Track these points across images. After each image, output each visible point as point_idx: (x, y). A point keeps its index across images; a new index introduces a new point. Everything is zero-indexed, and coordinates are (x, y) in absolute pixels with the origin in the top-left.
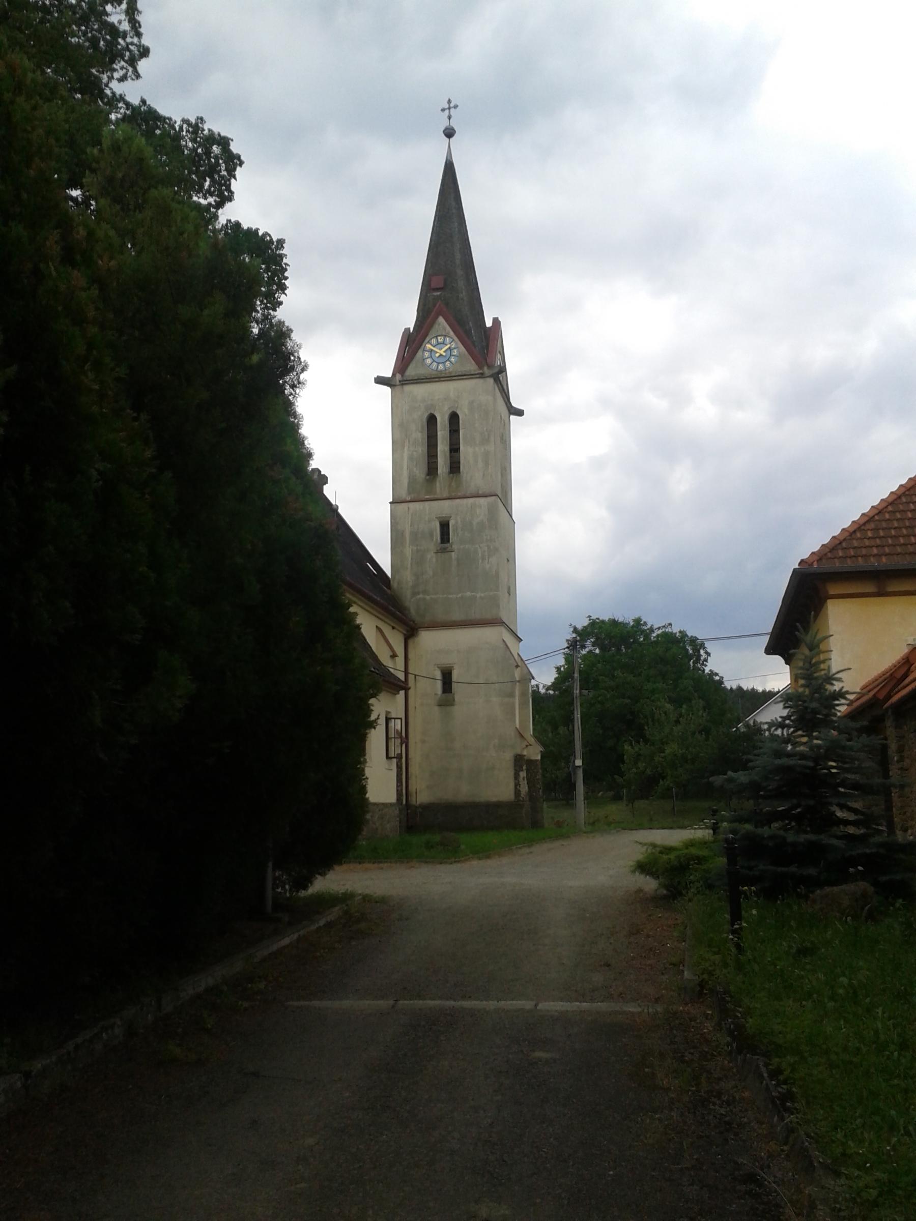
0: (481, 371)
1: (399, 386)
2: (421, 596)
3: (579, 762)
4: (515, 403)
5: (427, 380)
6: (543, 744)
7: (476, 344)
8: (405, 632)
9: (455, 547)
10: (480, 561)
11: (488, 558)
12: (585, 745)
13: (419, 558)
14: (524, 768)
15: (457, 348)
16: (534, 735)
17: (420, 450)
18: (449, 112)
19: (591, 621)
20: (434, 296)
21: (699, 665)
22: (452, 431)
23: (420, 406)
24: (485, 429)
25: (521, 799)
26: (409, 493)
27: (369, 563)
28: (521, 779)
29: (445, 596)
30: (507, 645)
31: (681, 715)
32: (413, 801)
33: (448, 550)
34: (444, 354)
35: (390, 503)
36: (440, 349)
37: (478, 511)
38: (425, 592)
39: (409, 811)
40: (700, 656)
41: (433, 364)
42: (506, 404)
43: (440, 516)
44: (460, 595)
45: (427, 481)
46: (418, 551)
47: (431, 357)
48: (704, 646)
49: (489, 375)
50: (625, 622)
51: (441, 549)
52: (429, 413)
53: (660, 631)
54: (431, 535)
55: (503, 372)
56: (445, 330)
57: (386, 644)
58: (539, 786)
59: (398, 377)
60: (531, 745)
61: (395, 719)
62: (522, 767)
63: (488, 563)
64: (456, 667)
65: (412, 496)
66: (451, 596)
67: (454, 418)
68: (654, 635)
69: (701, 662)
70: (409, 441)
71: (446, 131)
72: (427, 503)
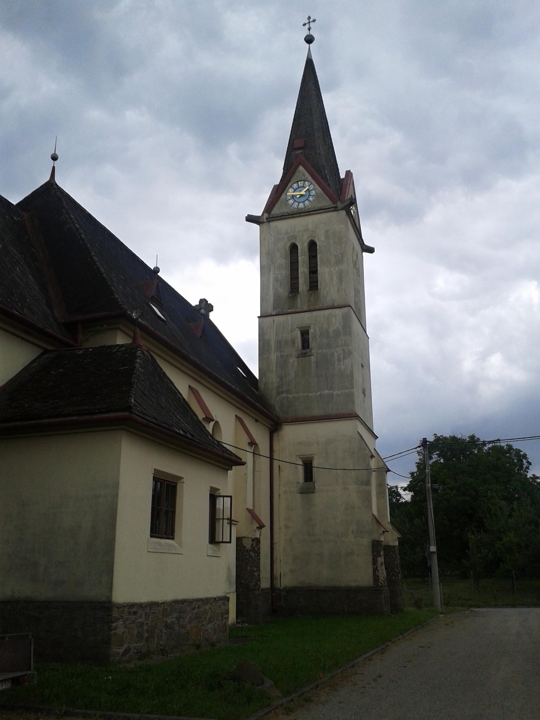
0: (334, 205)
1: (266, 223)
2: (285, 395)
3: (433, 549)
5: (290, 216)
6: (399, 530)
7: (331, 186)
8: (270, 427)
9: (314, 351)
10: (337, 363)
11: (344, 360)
12: (437, 533)
13: (283, 363)
14: (382, 553)
15: (315, 189)
16: (392, 523)
17: (284, 272)
18: (309, 26)
19: (437, 438)
20: (296, 153)
21: (522, 471)
22: (311, 257)
23: (283, 237)
24: (339, 252)
25: (380, 585)
26: (275, 308)
27: (239, 367)
28: (379, 564)
29: (306, 394)
30: (361, 437)
31: (513, 509)
32: (278, 585)
33: (308, 354)
35: (258, 317)
37: (334, 320)
38: (288, 392)
39: (274, 594)
40: (522, 464)
41: (295, 203)
42: (359, 240)
43: (301, 326)
44: (319, 393)
45: (290, 297)
46: (282, 356)
47: (295, 201)
48: (526, 456)
49: (341, 208)
50: (463, 438)
51: (301, 354)
52: (291, 242)
53: (490, 445)
54: (293, 342)
55: (354, 203)
56: (305, 176)
57: (244, 433)
58: (397, 570)
59: (266, 215)
60: (387, 531)
61: (224, 497)
62: (380, 553)
63: (343, 365)
64: (316, 458)
65: (277, 310)
66: (310, 394)
67: (312, 245)
68: (486, 448)
69: (524, 469)
70: (274, 266)
71: (308, 38)
72: (289, 316)
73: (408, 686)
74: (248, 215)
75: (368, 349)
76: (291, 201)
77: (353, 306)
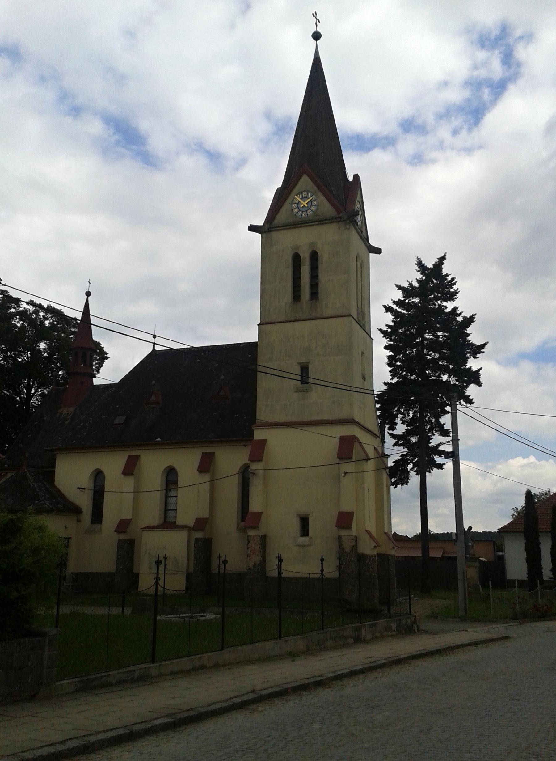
4: (373, 242)
34: (306, 205)
35: (258, 325)
36: (304, 202)
59: (267, 226)
73: (387, 707)
74: (250, 225)
75: (371, 353)
76: (294, 206)
77: (354, 313)
